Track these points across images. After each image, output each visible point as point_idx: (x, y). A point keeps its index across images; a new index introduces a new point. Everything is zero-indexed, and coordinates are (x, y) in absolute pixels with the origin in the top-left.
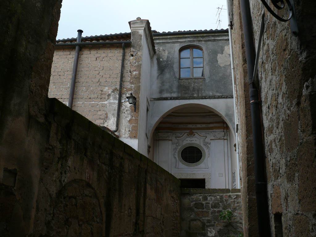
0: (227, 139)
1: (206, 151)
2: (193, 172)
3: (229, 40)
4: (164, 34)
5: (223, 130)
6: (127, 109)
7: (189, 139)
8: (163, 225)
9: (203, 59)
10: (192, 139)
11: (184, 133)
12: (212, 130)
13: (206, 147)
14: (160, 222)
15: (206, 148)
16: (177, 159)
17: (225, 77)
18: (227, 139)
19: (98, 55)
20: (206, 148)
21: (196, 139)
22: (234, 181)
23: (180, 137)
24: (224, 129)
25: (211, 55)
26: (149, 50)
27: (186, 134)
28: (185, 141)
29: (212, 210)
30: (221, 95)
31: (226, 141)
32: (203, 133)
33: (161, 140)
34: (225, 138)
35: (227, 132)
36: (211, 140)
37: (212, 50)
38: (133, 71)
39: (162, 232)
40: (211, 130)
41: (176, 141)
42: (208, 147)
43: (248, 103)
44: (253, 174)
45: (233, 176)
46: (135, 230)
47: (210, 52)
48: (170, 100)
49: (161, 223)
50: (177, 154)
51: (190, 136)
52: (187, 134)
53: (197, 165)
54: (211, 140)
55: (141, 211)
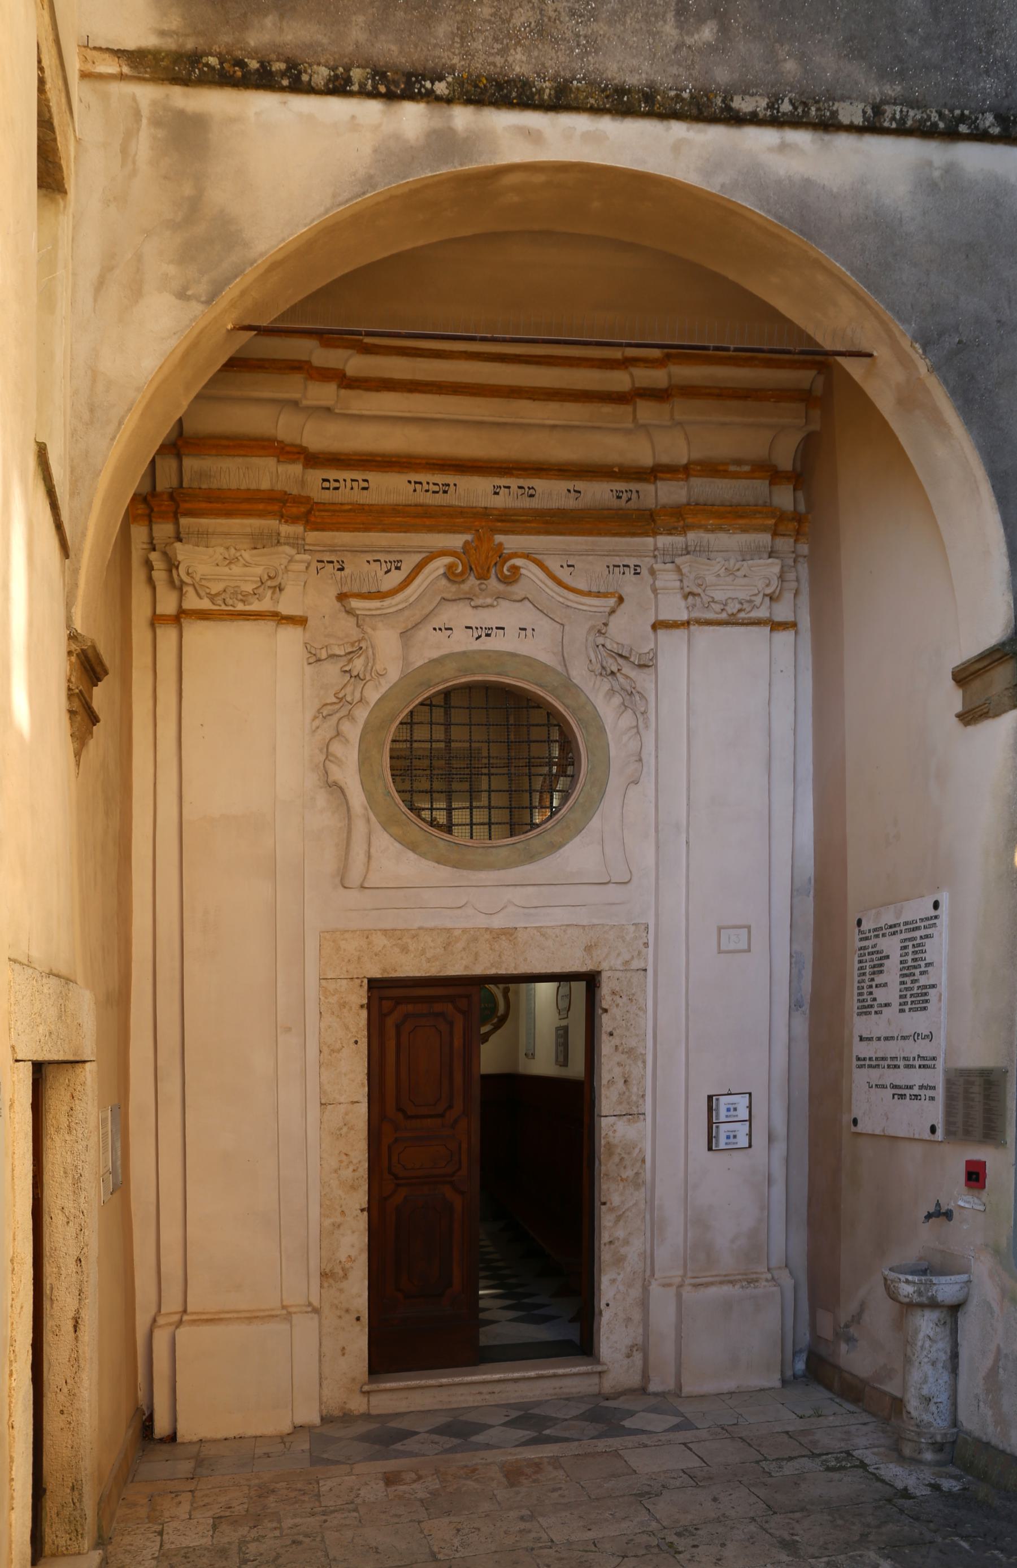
0: (793, 625)
1: (618, 746)
2: (498, 922)
5: (766, 538)
7: (460, 615)
9: (749, 932)
10: (489, 618)
11: (417, 558)
12: (678, 540)
13: (612, 691)
15: (617, 700)
16: (357, 798)
20: (617, 700)
21: (526, 615)
23: (380, 595)
24: (775, 534)
27: (440, 564)
28: (425, 632)
31: (785, 638)
32: (586, 558)
33: (203, 615)
34: (783, 612)
42: (631, 698)
50: (349, 755)
51: (472, 581)
52: (450, 567)
53: (531, 857)
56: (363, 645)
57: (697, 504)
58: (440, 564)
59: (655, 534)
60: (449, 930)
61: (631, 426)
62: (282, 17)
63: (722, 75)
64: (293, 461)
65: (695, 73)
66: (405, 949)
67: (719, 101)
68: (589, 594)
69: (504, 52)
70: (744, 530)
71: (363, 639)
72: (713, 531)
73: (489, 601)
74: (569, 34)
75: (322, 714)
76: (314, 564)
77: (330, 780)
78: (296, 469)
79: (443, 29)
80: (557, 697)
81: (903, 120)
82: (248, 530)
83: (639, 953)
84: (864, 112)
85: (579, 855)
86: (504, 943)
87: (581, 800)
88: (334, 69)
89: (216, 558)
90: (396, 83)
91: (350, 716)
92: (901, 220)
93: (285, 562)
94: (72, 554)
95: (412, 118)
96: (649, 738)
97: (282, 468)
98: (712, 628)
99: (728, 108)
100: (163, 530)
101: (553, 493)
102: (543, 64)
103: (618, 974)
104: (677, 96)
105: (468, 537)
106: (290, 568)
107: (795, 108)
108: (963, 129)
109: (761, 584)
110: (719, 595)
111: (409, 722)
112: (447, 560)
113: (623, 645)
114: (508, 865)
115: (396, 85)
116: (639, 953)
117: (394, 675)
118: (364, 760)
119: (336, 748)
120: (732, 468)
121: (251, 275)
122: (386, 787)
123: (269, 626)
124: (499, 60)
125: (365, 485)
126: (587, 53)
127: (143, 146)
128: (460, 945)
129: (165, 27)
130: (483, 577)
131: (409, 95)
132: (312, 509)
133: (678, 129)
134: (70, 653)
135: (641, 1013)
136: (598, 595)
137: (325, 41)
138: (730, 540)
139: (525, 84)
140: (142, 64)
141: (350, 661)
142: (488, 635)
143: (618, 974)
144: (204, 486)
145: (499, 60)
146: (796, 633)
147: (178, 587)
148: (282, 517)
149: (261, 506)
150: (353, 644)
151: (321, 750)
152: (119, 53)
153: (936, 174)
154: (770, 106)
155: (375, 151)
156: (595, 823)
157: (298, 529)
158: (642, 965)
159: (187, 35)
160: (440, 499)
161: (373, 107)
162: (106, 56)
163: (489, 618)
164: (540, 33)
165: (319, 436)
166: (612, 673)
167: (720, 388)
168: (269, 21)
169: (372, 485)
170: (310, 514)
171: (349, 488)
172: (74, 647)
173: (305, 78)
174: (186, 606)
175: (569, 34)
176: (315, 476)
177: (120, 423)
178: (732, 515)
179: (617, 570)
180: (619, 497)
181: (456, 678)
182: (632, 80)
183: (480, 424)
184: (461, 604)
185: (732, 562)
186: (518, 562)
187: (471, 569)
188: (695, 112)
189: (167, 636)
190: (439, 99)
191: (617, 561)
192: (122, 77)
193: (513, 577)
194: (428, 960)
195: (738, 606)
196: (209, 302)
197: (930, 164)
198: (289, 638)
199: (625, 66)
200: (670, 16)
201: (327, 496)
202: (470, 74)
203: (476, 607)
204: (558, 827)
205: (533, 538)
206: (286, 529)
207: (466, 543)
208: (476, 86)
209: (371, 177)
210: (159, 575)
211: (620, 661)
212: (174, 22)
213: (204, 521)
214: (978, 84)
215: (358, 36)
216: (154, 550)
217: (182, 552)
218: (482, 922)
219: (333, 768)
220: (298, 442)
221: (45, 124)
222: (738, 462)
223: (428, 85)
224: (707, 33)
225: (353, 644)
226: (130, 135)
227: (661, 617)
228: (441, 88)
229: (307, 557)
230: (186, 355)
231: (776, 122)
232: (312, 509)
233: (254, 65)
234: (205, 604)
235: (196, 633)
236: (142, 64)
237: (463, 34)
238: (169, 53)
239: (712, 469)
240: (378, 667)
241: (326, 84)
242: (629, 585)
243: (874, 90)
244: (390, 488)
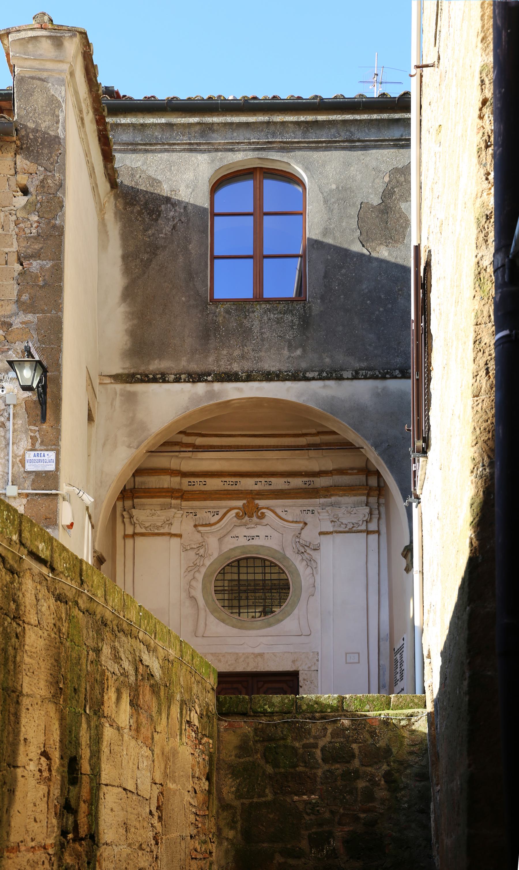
2: (257, 651)
3: (409, 125)
4: (150, 107)
5: (364, 498)
7: (242, 531)
8: (160, 818)
9: (359, 655)
11: (225, 510)
14: (148, 811)
15: (304, 563)
18: (378, 532)
19: (199, 795)
21: (267, 531)
23: (210, 525)
24: (368, 495)
26: (92, 174)
27: (233, 513)
28: (228, 539)
29: (326, 767)
31: (373, 537)
32: (292, 508)
33: (142, 535)
34: (373, 526)
35: (379, 505)
36: (321, 533)
37: (337, 188)
39: (157, 844)
40: (322, 500)
41: (198, 537)
45: (396, 660)
46: (64, 833)
48: (174, 382)
49: (151, 813)
50: (198, 585)
51: (246, 518)
52: (237, 514)
53: (270, 625)
54: (321, 533)
56: (204, 544)
57: (335, 486)
58: (233, 513)
59: (320, 498)
60: (237, 654)
61: (307, 457)
62: (160, 360)
63: (304, 365)
64: (177, 476)
65: (294, 365)
66: (220, 661)
67: (301, 374)
68: (292, 522)
69: (230, 364)
71: (204, 541)
72: (342, 496)
73: (253, 526)
74: (252, 357)
75: (188, 570)
76: (185, 514)
77: (191, 596)
78: (177, 479)
79: (211, 359)
80: (281, 563)
81: (366, 375)
82: (159, 503)
83: (315, 664)
84: (352, 374)
85: (289, 624)
86: (259, 659)
87: (290, 602)
88: (176, 375)
89: (147, 514)
90: (195, 378)
91: (198, 571)
92: (367, 407)
93: (173, 515)
94: (95, 527)
95: (201, 388)
96: (318, 578)
97: (172, 479)
98: (342, 534)
99: (305, 377)
100: (128, 503)
101: (278, 483)
102: (244, 367)
103: (306, 672)
104: (287, 374)
105: (245, 502)
106: (175, 516)
107: (328, 375)
108: (388, 376)
109: (361, 516)
110: (345, 521)
111: (223, 572)
113: (306, 541)
114: (260, 628)
115: (195, 378)
116: (315, 664)
117: (216, 555)
118: (204, 588)
119: (194, 583)
120: (349, 471)
121: (150, 438)
122: (213, 598)
123: (167, 538)
124: (229, 367)
125: (205, 483)
126: (258, 362)
127: (118, 399)
128: (242, 659)
129: (125, 366)
130: (251, 516)
131: (199, 381)
132: (183, 494)
133: (288, 384)
134: (94, 557)
135: (316, 688)
136: (296, 522)
137: (174, 366)
138: (348, 500)
139: (236, 374)
140: (117, 378)
141: (199, 550)
142: (253, 539)
143: (306, 672)
144: (143, 487)
145: (229, 367)
146: (379, 535)
147: (134, 525)
148: (172, 497)
149: (164, 494)
150: (199, 544)
151: (187, 584)
152: (110, 376)
153: (379, 391)
154: (319, 375)
155: (189, 399)
156: (296, 611)
157: (179, 501)
158: (316, 669)
159: (131, 368)
160: (234, 487)
161: (189, 385)
162: (107, 378)
164: (243, 357)
165: (187, 466)
166: (302, 553)
167: (341, 443)
168: (156, 362)
169: (207, 483)
170: (182, 495)
171: (199, 484)
172: (95, 555)
173: (167, 379)
174: (136, 531)
175: (252, 357)
177: (110, 486)
179: (305, 512)
180: (305, 484)
181: (240, 556)
182: (273, 369)
183: (249, 459)
184: (242, 527)
185: (349, 508)
187: (246, 514)
188: (293, 378)
189: (129, 542)
190: (209, 381)
191: (305, 508)
192: (111, 383)
194: (229, 665)
195: (352, 525)
196: (137, 448)
197: (377, 387)
198: (175, 542)
199: (270, 365)
200: (286, 348)
201: (190, 488)
202: (220, 372)
203: (248, 528)
204: (281, 613)
205: (271, 501)
206: (174, 502)
207: (244, 504)
208: (221, 377)
209: (188, 407)
210: (127, 520)
211: (306, 547)
212: (127, 365)
213: (143, 500)
214: (394, 360)
215: (184, 364)
216: (125, 510)
217: (134, 512)
218: (250, 650)
219: (192, 591)
220: (179, 469)
221: (90, 410)
222: (352, 469)
223: (205, 378)
224: (299, 352)
225: (199, 544)
226: (113, 399)
227: (322, 530)
228: (209, 378)
229: (182, 512)
230: (130, 464)
231: (321, 379)
232: (183, 494)
233: (151, 376)
234: (143, 531)
235: (139, 540)
236: (117, 378)
237: (217, 360)
238: (125, 374)
239: (341, 472)
240: (210, 552)
241: (173, 380)
242: (309, 518)
243: (357, 365)
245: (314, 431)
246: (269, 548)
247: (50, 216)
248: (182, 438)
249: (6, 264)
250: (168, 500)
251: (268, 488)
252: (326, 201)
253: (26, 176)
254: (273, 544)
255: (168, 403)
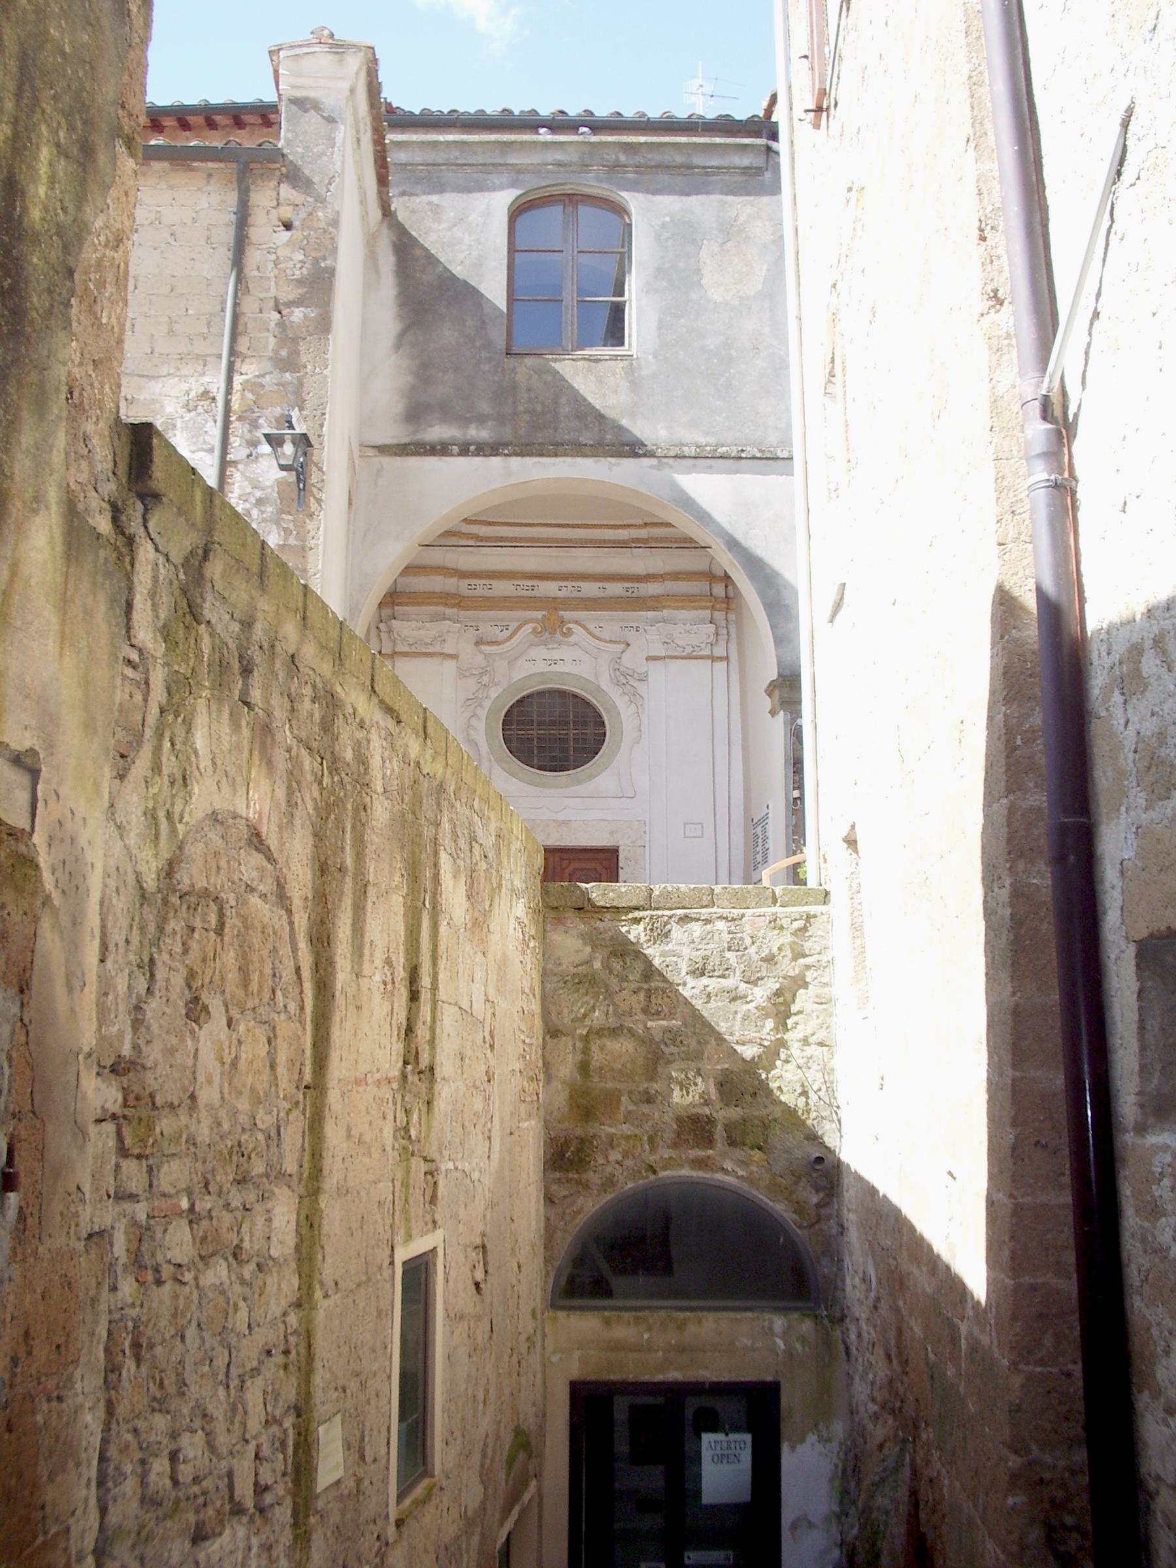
0: (727, 658)
2: (561, 817)
6: (258, 494)
7: (540, 653)
10: (556, 655)
11: (517, 624)
15: (626, 698)
17: (734, 354)
20: (626, 698)
22: (759, 858)
25: (670, 242)
27: (528, 628)
30: (711, 440)
31: (721, 666)
32: (610, 624)
33: (405, 654)
34: (719, 651)
36: (649, 658)
37: (672, 220)
38: (289, 304)
43: (1005, 483)
44: (1031, 785)
45: (756, 836)
47: (664, 226)
50: (481, 725)
51: (547, 635)
52: (534, 630)
53: (579, 782)
54: (649, 658)
55: (425, 981)
68: (610, 642)
70: (695, 608)
91: (480, 705)
101: (590, 589)
112: (533, 625)
118: (488, 728)
119: (474, 721)
136: (615, 642)
152: (373, 447)
157: (455, 610)
160: (530, 593)
163: (556, 655)
171: (481, 588)
176: (464, 583)
178: (688, 601)
186: (570, 625)
193: (570, 632)
207: (544, 616)
210: (384, 635)
219: (472, 732)
234: (406, 649)
236: (382, 449)
242: (631, 636)
244: (503, 588)
245: (640, 522)
246: (578, 677)
247: (319, 255)
248: (471, 530)
249: (261, 312)
250: (441, 609)
251: (576, 594)
252: (658, 237)
253: (290, 208)
254: (583, 670)
255: (462, 483)
